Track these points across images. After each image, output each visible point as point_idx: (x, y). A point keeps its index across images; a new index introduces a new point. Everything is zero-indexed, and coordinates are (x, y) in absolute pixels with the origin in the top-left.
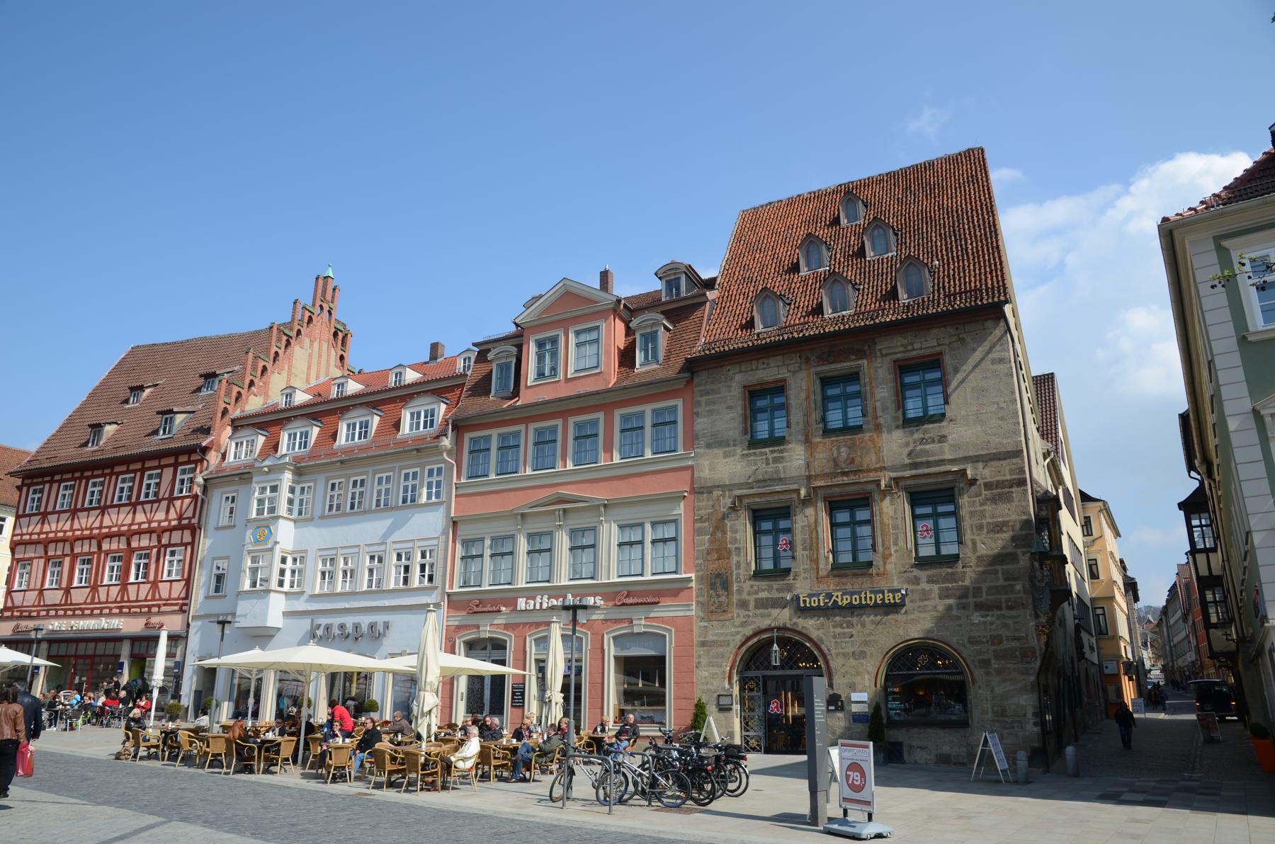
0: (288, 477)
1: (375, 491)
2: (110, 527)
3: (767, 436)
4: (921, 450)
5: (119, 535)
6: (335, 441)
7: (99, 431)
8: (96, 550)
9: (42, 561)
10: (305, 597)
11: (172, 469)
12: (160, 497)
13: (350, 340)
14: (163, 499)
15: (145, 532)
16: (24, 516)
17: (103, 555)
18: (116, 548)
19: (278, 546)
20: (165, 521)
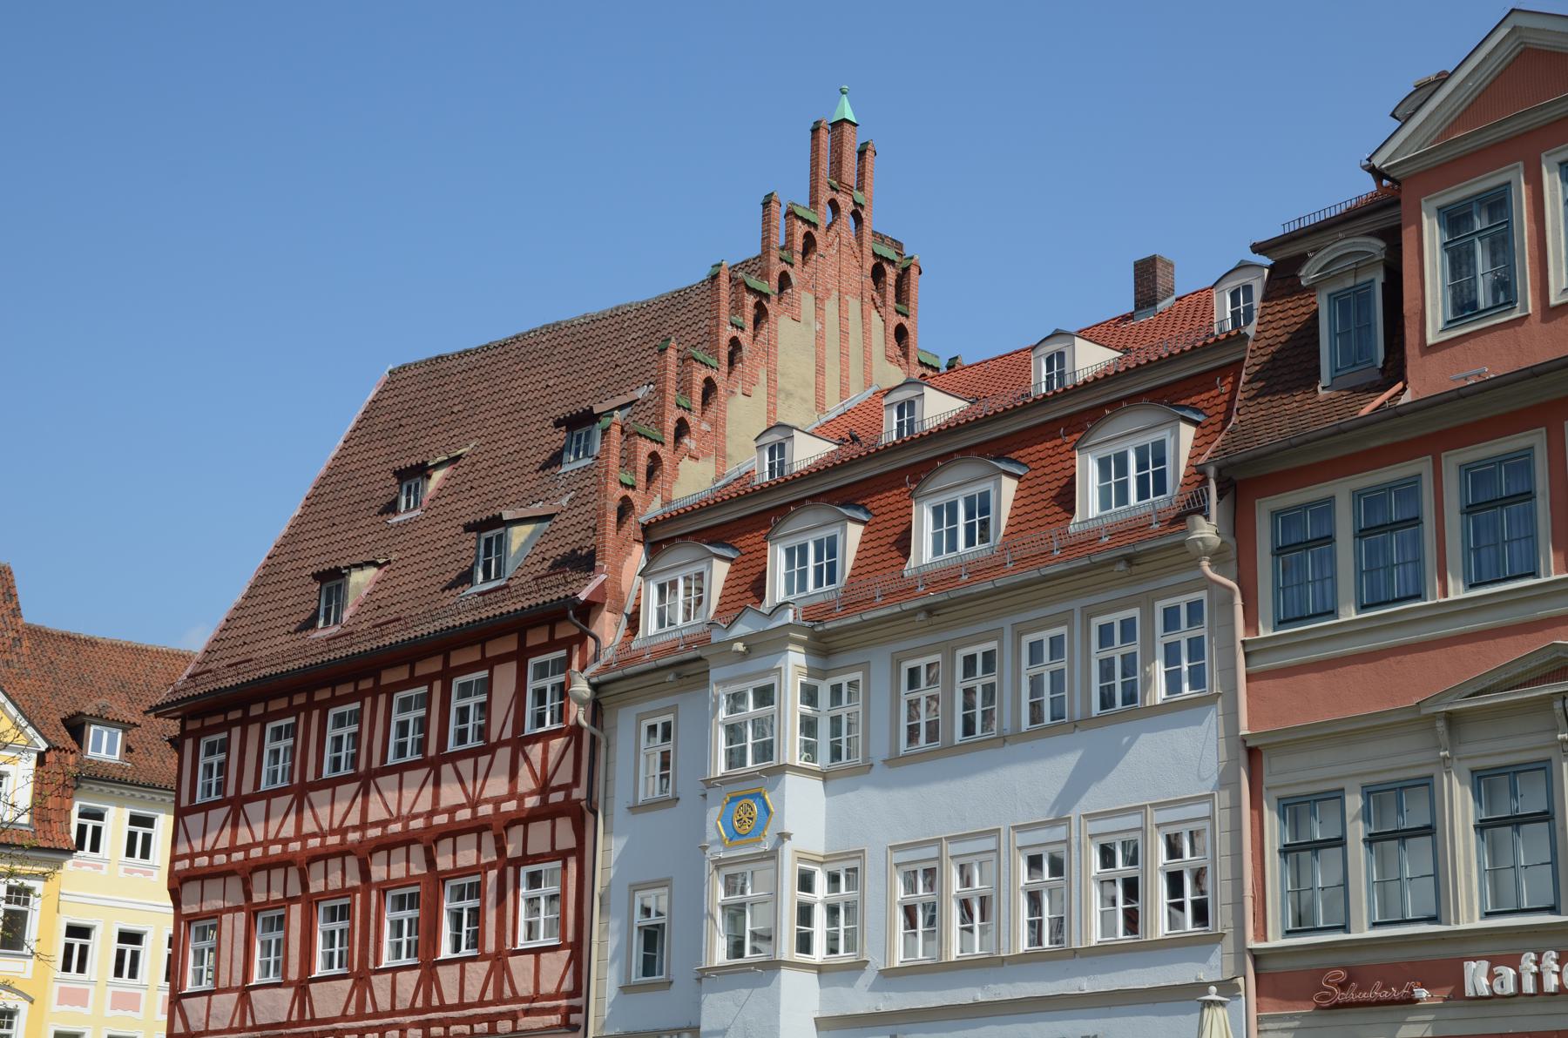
0: (795, 660)
2: (383, 824)
10: (869, 976)
13: (919, 287)
14: (501, 743)
17: (374, 893)
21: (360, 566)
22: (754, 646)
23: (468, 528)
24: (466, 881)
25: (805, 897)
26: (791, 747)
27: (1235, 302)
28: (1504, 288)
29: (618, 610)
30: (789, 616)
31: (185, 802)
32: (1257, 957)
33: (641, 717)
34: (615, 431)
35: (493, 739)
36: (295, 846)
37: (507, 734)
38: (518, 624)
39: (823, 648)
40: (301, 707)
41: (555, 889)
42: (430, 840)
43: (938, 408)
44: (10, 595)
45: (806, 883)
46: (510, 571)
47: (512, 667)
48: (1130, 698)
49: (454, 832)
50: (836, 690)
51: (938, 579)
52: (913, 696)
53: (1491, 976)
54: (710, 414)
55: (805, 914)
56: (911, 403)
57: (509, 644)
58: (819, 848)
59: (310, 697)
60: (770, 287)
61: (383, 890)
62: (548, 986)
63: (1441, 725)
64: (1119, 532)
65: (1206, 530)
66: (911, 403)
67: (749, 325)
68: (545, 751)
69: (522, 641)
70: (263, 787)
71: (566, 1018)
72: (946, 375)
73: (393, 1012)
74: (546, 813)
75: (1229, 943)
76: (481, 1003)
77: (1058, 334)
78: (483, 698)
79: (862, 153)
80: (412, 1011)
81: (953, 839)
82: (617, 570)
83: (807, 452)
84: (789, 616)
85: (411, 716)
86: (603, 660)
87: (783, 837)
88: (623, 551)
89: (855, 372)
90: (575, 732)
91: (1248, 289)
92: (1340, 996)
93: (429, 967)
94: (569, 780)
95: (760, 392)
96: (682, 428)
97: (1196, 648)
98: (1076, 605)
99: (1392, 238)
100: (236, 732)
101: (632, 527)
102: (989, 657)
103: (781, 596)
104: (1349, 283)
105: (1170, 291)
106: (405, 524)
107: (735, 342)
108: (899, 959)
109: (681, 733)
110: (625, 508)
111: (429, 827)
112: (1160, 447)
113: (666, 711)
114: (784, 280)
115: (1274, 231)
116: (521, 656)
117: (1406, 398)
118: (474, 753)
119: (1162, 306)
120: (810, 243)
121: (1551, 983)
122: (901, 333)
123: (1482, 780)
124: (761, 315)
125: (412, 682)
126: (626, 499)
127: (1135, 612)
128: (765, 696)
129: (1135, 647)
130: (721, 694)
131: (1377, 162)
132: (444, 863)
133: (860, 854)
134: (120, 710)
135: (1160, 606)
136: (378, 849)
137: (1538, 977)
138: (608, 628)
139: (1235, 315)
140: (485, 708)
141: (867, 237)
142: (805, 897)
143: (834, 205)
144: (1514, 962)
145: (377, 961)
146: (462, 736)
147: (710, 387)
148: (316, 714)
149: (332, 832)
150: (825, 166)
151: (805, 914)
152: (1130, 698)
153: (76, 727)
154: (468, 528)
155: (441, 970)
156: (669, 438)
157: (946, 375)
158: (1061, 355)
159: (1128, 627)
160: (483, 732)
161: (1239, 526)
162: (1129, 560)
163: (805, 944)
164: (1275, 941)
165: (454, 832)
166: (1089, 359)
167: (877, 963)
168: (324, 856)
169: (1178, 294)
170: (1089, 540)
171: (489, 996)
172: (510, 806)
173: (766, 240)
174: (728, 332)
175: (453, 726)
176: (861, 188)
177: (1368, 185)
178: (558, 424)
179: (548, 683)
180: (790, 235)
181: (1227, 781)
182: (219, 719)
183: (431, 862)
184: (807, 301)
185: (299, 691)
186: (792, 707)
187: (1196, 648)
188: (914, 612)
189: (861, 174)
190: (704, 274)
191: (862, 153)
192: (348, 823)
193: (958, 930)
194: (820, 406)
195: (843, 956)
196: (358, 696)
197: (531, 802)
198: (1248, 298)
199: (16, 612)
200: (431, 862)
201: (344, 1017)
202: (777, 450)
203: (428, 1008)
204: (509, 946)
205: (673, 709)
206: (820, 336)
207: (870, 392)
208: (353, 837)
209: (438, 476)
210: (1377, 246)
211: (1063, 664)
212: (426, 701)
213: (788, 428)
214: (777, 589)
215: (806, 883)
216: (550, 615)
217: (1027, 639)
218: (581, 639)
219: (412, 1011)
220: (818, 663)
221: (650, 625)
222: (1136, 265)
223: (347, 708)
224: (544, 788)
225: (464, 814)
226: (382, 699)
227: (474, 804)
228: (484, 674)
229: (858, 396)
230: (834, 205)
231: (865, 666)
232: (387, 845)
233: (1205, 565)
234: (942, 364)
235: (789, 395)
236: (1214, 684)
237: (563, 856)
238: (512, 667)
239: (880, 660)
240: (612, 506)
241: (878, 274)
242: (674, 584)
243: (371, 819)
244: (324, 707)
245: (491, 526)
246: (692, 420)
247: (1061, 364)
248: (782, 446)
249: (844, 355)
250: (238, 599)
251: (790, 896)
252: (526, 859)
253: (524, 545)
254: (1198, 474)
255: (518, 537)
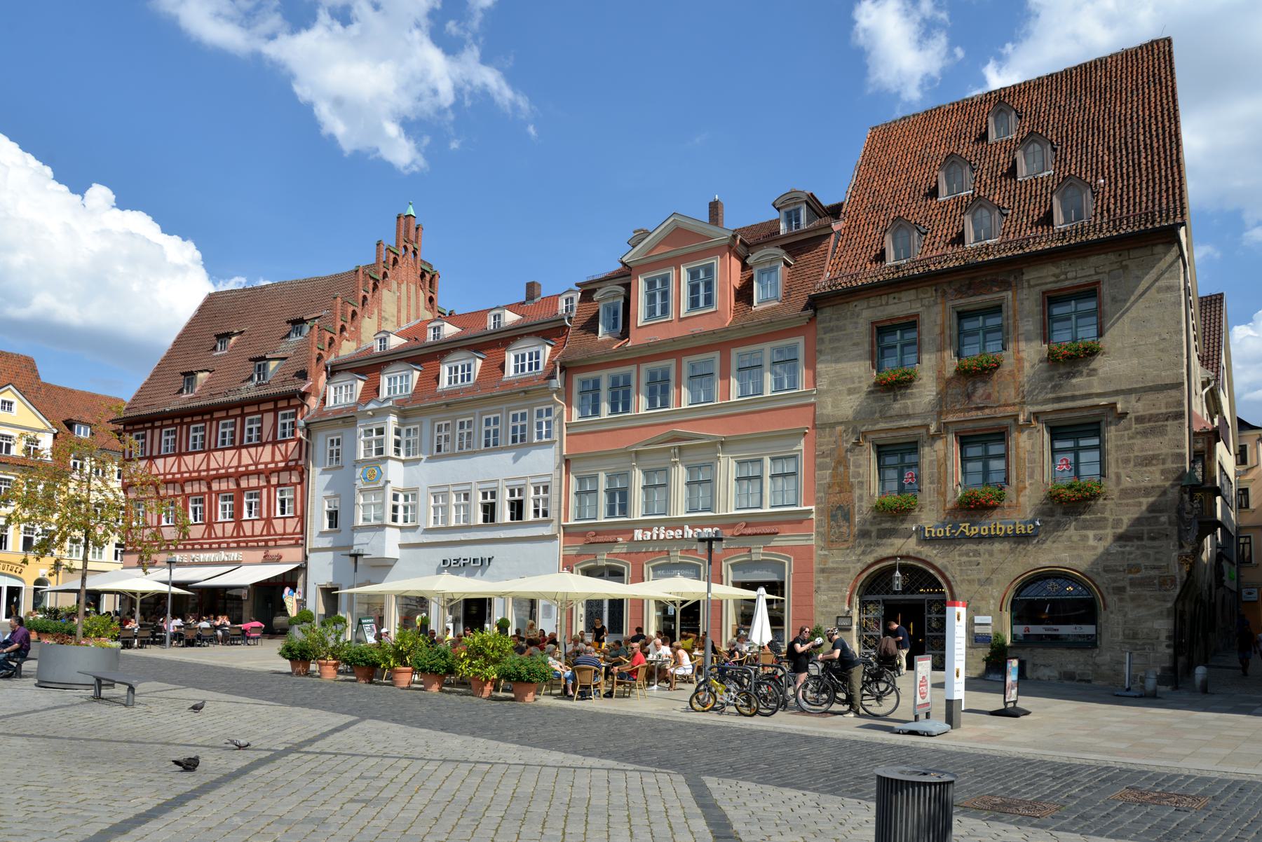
0: (392, 421)
2: (217, 470)
10: (420, 530)
13: (439, 283)
14: (267, 443)
21: (201, 371)
22: (376, 413)
23: (251, 360)
24: (253, 492)
25: (395, 503)
26: (390, 450)
27: (567, 303)
28: (665, 310)
29: (317, 396)
30: (391, 403)
32: (564, 527)
33: (327, 436)
34: (316, 328)
35: (264, 440)
36: (178, 476)
37: (270, 439)
38: (275, 399)
40: (178, 424)
41: (292, 496)
42: (238, 477)
43: (449, 330)
44: (34, 370)
45: (395, 497)
46: (269, 377)
47: (271, 415)
48: (523, 437)
49: (248, 474)
50: (409, 431)
51: (447, 393)
53: (643, 534)
54: (354, 324)
55: (395, 509)
56: (439, 327)
57: (271, 406)
58: (401, 486)
59: (182, 420)
60: (379, 277)
61: (218, 493)
62: (289, 530)
63: (633, 455)
64: (520, 381)
65: (557, 383)
66: (439, 327)
67: (371, 290)
68: (287, 447)
69: (276, 405)
70: (162, 453)
71: (297, 541)
72: (451, 317)
73: (253, 536)
74: (287, 469)
75: (556, 523)
76: (261, 535)
77: (497, 308)
78: (259, 425)
79: (417, 229)
80: (232, 537)
81: (453, 485)
82: (317, 381)
83: (395, 342)
84: (391, 403)
85: (228, 430)
86: (311, 414)
87: (388, 482)
88: (318, 374)
89: (413, 311)
90: (300, 440)
91: (572, 299)
92: (592, 540)
93: (239, 522)
95: (375, 317)
96: (343, 329)
97: (549, 424)
98: (504, 407)
99: (627, 286)
100: (149, 432)
101: (322, 365)
102: (469, 422)
103: (386, 395)
104: (611, 301)
105: (539, 295)
106: (220, 356)
107: (365, 298)
108: (431, 525)
109: (344, 442)
110: (320, 358)
111: (237, 472)
112: (538, 353)
113: (338, 434)
114: (385, 275)
115: (584, 280)
116: (275, 410)
117: (629, 344)
118: (256, 446)
119: (536, 300)
120: (395, 261)
121: (662, 537)
122: (431, 299)
123: (646, 473)
124: (375, 287)
125: (228, 417)
126: (320, 354)
127: (526, 410)
128: (380, 431)
129: (526, 422)
130: (361, 430)
131: (624, 260)
132: (244, 484)
133: (417, 489)
134: (87, 418)
135: (535, 409)
136: (274, 472)
137: (658, 535)
138: (313, 402)
139: (567, 308)
140: (260, 429)
141: (419, 262)
142: (395, 503)
143: (405, 247)
144: (651, 530)
145: (216, 518)
146: (195, 446)
147: (354, 314)
148: (185, 427)
149: (194, 471)
150: (402, 232)
151: (395, 509)
152: (495, 444)
153: (70, 424)
154: (251, 360)
155: (244, 523)
156: (338, 332)
157: (451, 317)
158: (499, 315)
159: (523, 416)
160: (259, 438)
161: (567, 383)
162: (525, 392)
163: (395, 519)
164: (571, 522)
165: (248, 474)
166: (510, 318)
167: (423, 526)
168: (191, 480)
169: (543, 296)
170: (510, 383)
171: (265, 533)
172: (272, 466)
173: (378, 258)
174: (362, 293)
175: (246, 435)
176: (417, 242)
177: (621, 266)
178: (288, 322)
179: (287, 421)
180: (388, 257)
181: (559, 467)
182: (141, 426)
183: (238, 485)
184: (394, 285)
185: (177, 417)
186: (390, 437)
187: (549, 424)
188: (441, 405)
189: (417, 237)
190: (353, 268)
191: (417, 229)
192: (201, 468)
193: (733, 484)
194: (399, 324)
195: (409, 524)
196: (203, 421)
197: (282, 465)
198: (572, 302)
199: (38, 377)
200: (238, 485)
201: (203, 538)
202: (383, 340)
203: (238, 536)
204: (272, 515)
205: (341, 434)
206: (399, 298)
207: (418, 321)
208: (204, 474)
209: (234, 339)
210: (622, 290)
211: (498, 427)
212: (234, 425)
213: (388, 333)
214: (384, 393)
215: (395, 497)
216: (289, 396)
217: (484, 418)
218: (302, 406)
219: (232, 537)
220: (402, 420)
221: (330, 402)
223: (199, 425)
224: (286, 459)
225: (253, 468)
226: (214, 423)
227: (256, 464)
228: (260, 416)
229: (413, 322)
230: (405, 247)
231: (420, 423)
232: (219, 478)
233: (555, 395)
234: (447, 313)
235: (386, 319)
236: (556, 436)
237: (295, 485)
238: (271, 415)
239: (426, 421)
240: (315, 356)
241: (422, 276)
242: (341, 388)
243: (211, 467)
244: (188, 424)
245: (260, 361)
246: (347, 326)
247: (499, 318)
248: (385, 339)
249: (409, 306)
250: (146, 380)
251: (390, 502)
252: (279, 485)
253: (275, 368)
254: (552, 362)
255: (272, 365)
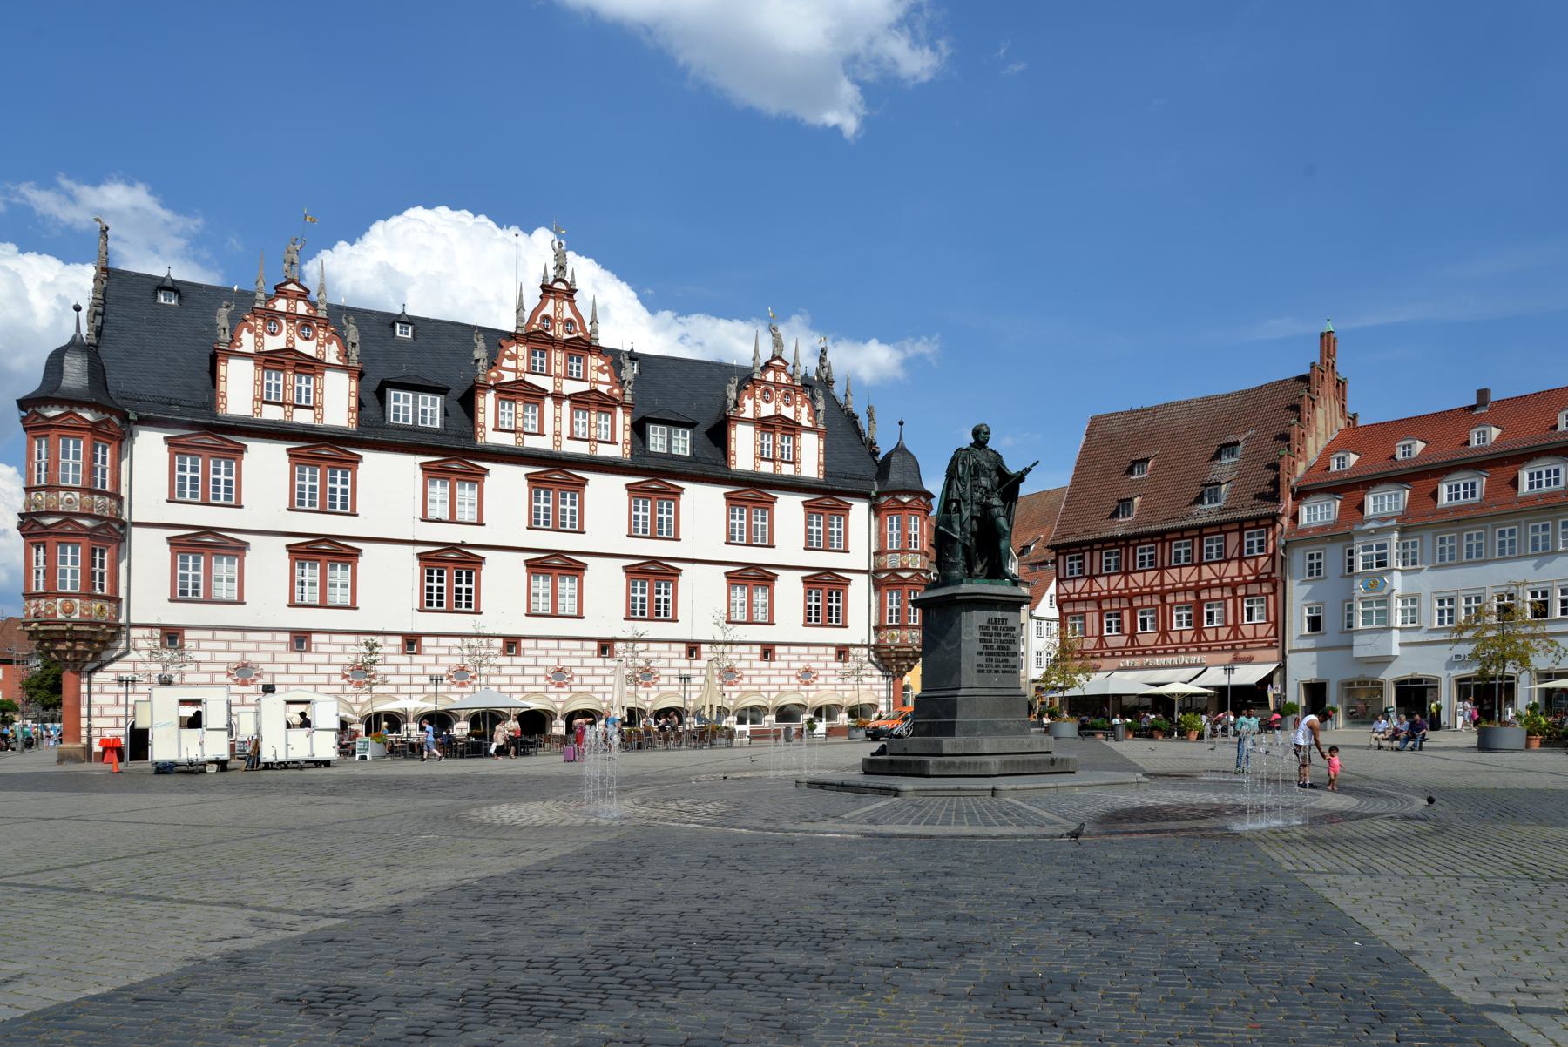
0: (1396, 535)
1: (1465, 547)
2: (1099, 592)
3: (652, 449)
4: (875, 656)
5: (1185, 590)
6: (1436, 501)
7: (1129, 505)
8: (1159, 602)
9: (1096, 616)
10: (1423, 630)
11: (1237, 534)
12: (1228, 557)
13: (1349, 388)
14: (1232, 559)
15: (1216, 586)
16: (1065, 579)
17: (1168, 607)
18: (1183, 600)
19: (1395, 593)
20: (1239, 576)
31: (1061, 576)
37: (1236, 555)
39: (1403, 531)
52: (1442, 546)
61: (1172, 605)
74: (1222, 586)
94: (1270, 570)
205: (1324, 549)
222: (1095, 422)
